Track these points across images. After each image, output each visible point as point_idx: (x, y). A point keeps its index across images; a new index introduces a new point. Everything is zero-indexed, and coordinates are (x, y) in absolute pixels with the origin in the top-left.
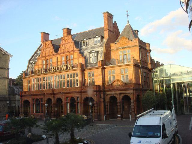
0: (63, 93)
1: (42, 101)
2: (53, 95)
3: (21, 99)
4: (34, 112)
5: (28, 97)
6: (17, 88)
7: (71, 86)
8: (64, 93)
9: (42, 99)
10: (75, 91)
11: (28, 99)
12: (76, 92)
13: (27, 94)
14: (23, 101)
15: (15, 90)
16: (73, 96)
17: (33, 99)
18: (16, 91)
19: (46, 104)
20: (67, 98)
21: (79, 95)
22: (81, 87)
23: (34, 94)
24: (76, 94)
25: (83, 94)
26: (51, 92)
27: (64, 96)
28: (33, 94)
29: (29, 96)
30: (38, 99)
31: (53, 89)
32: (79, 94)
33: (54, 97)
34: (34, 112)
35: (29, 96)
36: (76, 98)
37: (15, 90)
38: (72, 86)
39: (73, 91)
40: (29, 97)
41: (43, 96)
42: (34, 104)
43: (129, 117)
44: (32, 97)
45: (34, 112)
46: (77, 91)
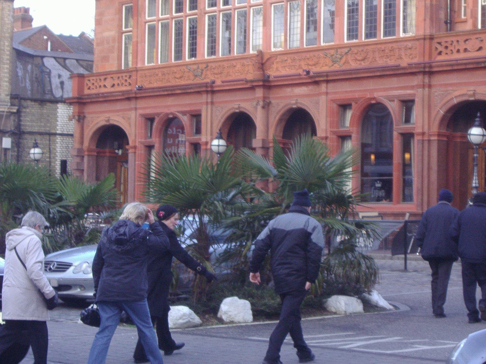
0: (319, 74)
1: (198, 131)
2: (259, 93)
3: (80, 118)
4: (49, 49)
5: (119, 106)
6: (65, 67)
7: (371, 32)
8: (327, 74)
9: (196, 117)
10: (391, 62)
11: (117, 120)
12: (398, 67)
13: (117, 89)
14: (89, 132)
15: (49, 73)
16: (376, 95)
17: (150, 119)
18: (55, 81)
19: (215, 142)
20: (345, 106)
21: (418, 86)
22: (431, 38)
23: (155, 85)
24: (394, 82)
25: (437, 80)
26: (252, 74)
27: (323, 98)
28: (146, 85)
29: (128, 98)
30: (175, 118)
31: (260, 54)
32: (417, 80)
33: (267, 106)
34: (49, 49)
35: (128, 98)
36: (393, 107)
37: (54, 73)
38: (356, 37)
39: (381, 62)
40: (125, 105)
41: (205, 98)
42: (150, 148)
43: (152, 16)
44: (141, 104)
45: (47, 49)
46: (404, 63)
